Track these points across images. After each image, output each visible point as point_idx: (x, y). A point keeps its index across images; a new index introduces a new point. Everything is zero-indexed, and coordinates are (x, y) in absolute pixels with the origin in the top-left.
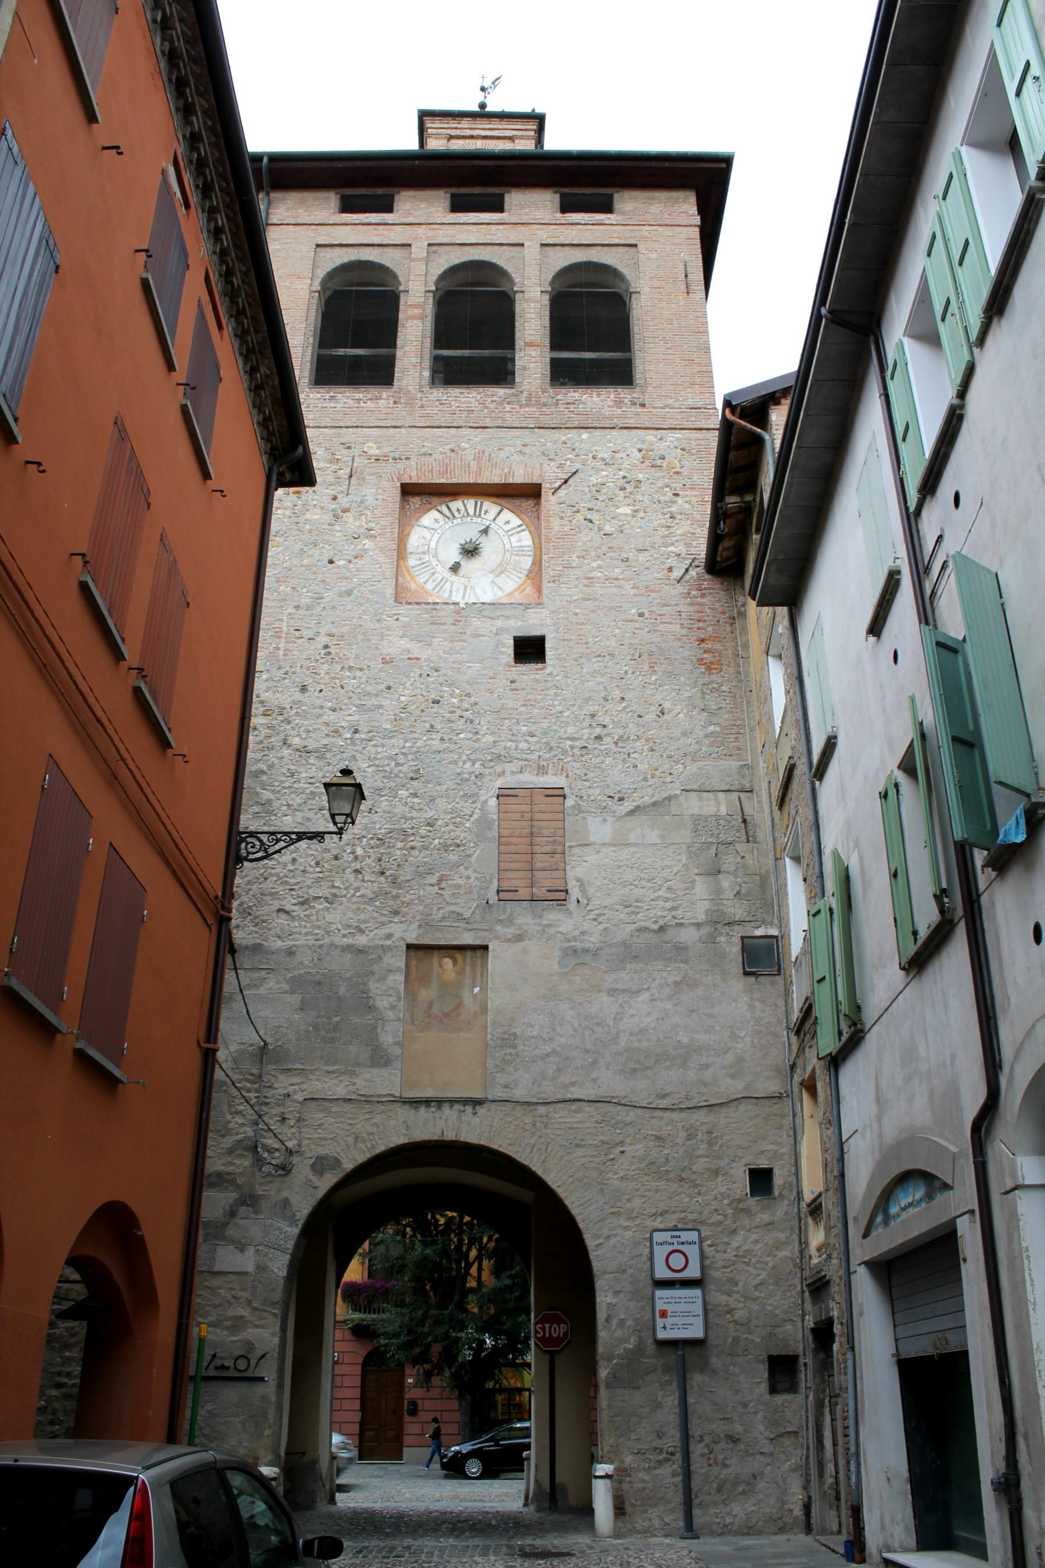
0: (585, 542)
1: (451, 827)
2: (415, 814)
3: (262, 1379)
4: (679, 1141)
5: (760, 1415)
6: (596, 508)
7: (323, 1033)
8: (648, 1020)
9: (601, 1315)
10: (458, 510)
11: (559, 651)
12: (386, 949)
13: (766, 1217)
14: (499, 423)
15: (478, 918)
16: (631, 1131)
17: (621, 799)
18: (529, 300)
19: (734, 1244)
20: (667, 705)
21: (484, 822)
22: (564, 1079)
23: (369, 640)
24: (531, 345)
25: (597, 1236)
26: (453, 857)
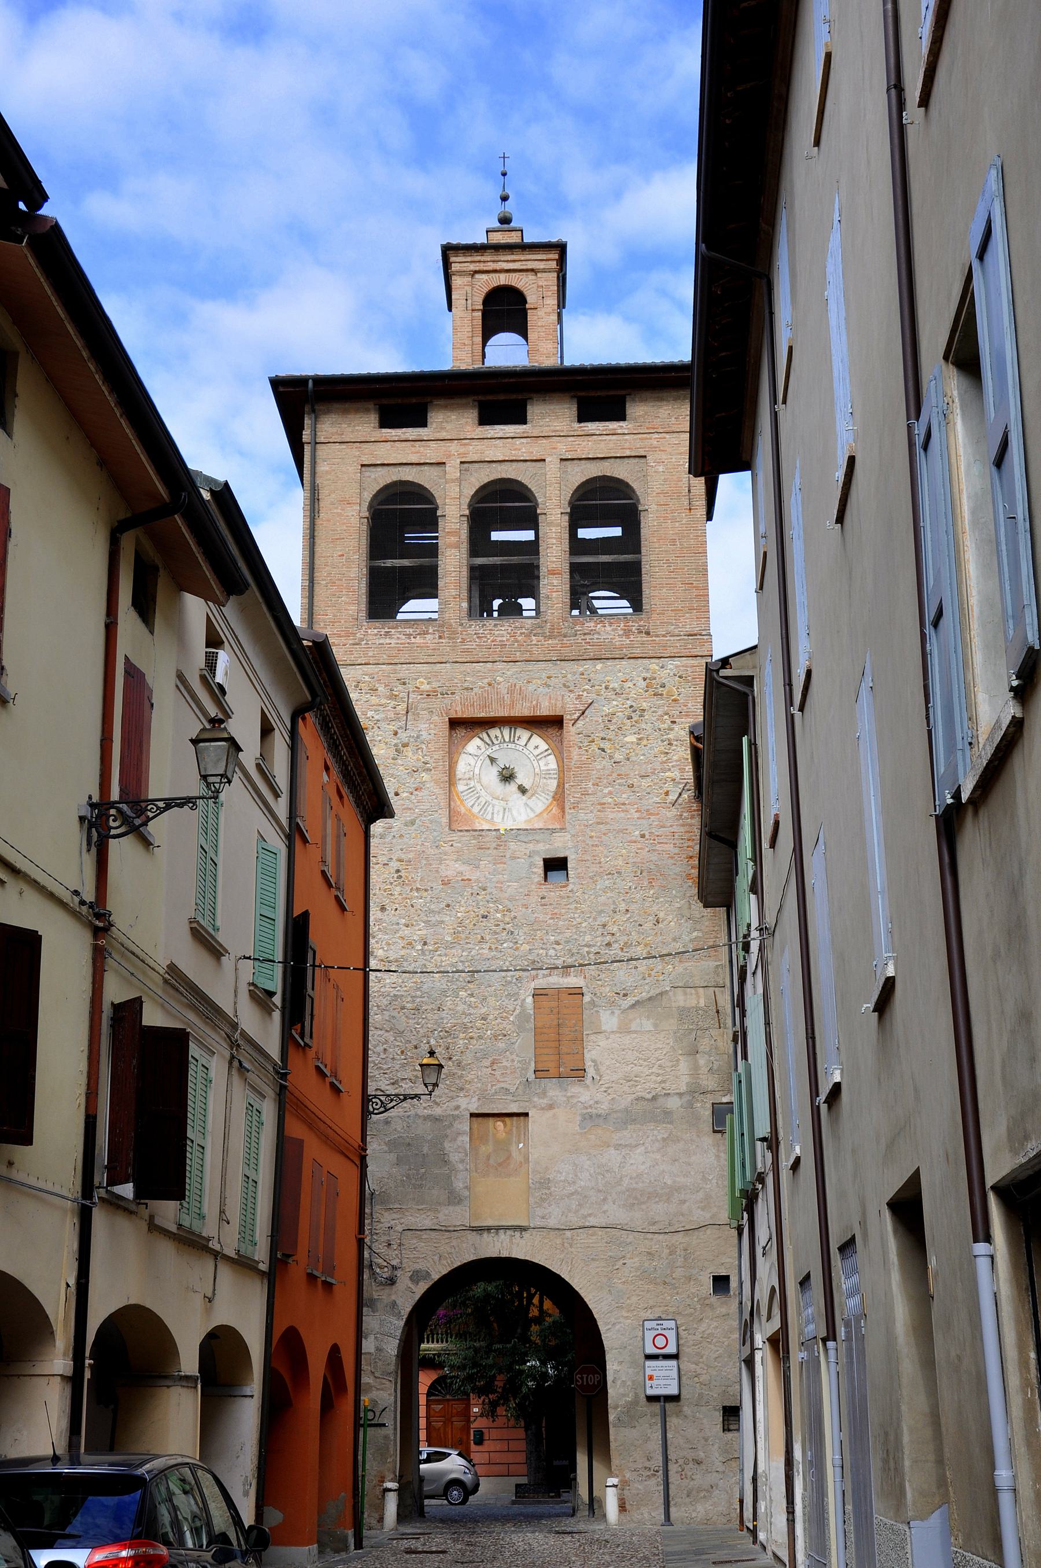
0: (598, 770)
1: (499, 1020)
2: (472, 1011)
3: (384, 1425)
4: (664, 1255)
5: (716, 1446)
6: (608, 737)
7: (413, 1181)
8: (643, 1167)
9: (610, 1378)
10: (496, 737)
11: (579, 870)
12: (455, 1118)
13: (723, 1310)
14: (527, 656)
15: (520, 1091)
16: (631, 1248)
17: (625, 995)
18: (550, 524)
19: (701, 1329)
20: (661, 915)
21: (523, 1016)
22: (584, 1211)
23: (430, 865)
24: (552, 572)
25: (607, 1324)
26: (501, 1045)
